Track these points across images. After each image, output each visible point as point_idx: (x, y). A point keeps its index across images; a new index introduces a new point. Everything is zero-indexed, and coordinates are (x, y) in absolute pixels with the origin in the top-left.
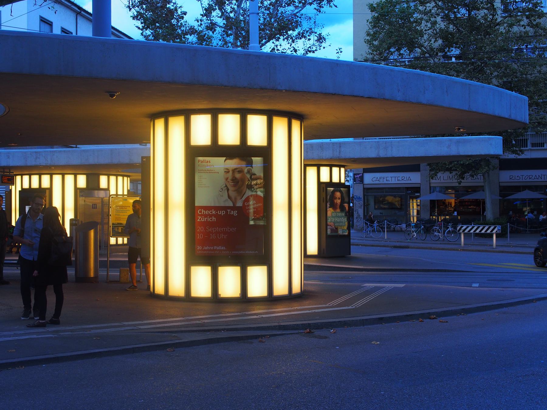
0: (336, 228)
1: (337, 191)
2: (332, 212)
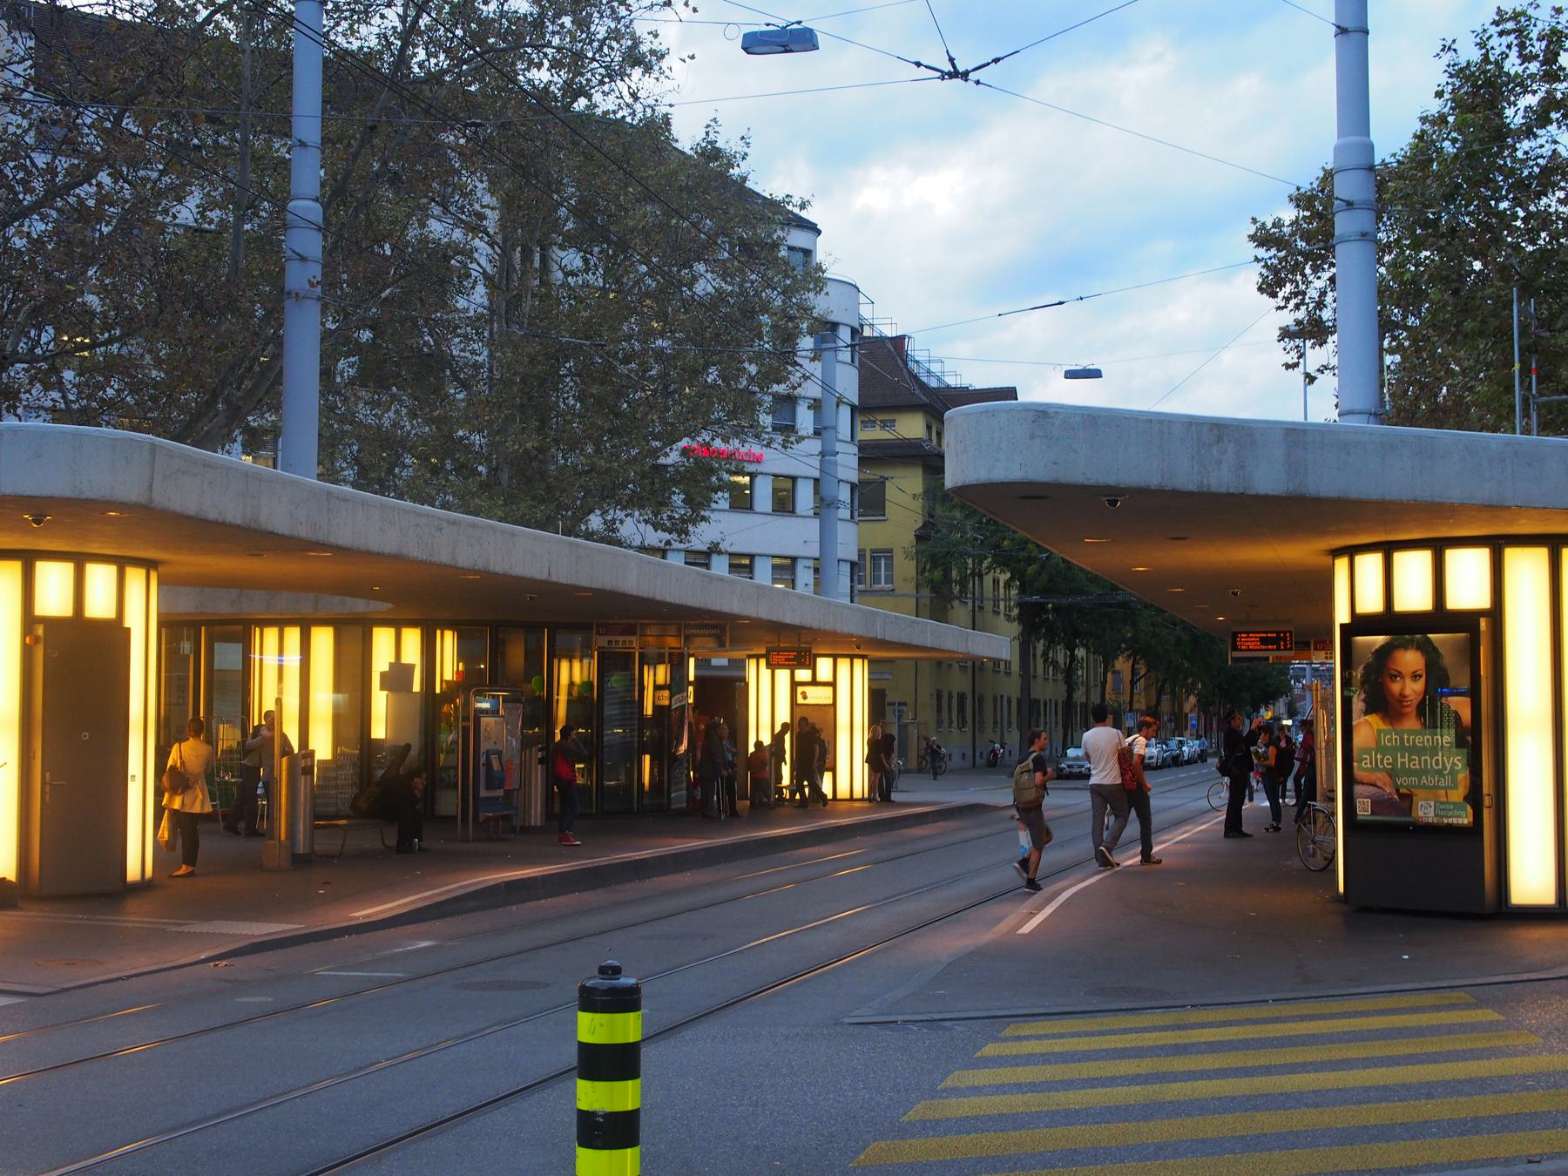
0: (1401, 796)
1: (1405, 646)
2: (1379, 731)
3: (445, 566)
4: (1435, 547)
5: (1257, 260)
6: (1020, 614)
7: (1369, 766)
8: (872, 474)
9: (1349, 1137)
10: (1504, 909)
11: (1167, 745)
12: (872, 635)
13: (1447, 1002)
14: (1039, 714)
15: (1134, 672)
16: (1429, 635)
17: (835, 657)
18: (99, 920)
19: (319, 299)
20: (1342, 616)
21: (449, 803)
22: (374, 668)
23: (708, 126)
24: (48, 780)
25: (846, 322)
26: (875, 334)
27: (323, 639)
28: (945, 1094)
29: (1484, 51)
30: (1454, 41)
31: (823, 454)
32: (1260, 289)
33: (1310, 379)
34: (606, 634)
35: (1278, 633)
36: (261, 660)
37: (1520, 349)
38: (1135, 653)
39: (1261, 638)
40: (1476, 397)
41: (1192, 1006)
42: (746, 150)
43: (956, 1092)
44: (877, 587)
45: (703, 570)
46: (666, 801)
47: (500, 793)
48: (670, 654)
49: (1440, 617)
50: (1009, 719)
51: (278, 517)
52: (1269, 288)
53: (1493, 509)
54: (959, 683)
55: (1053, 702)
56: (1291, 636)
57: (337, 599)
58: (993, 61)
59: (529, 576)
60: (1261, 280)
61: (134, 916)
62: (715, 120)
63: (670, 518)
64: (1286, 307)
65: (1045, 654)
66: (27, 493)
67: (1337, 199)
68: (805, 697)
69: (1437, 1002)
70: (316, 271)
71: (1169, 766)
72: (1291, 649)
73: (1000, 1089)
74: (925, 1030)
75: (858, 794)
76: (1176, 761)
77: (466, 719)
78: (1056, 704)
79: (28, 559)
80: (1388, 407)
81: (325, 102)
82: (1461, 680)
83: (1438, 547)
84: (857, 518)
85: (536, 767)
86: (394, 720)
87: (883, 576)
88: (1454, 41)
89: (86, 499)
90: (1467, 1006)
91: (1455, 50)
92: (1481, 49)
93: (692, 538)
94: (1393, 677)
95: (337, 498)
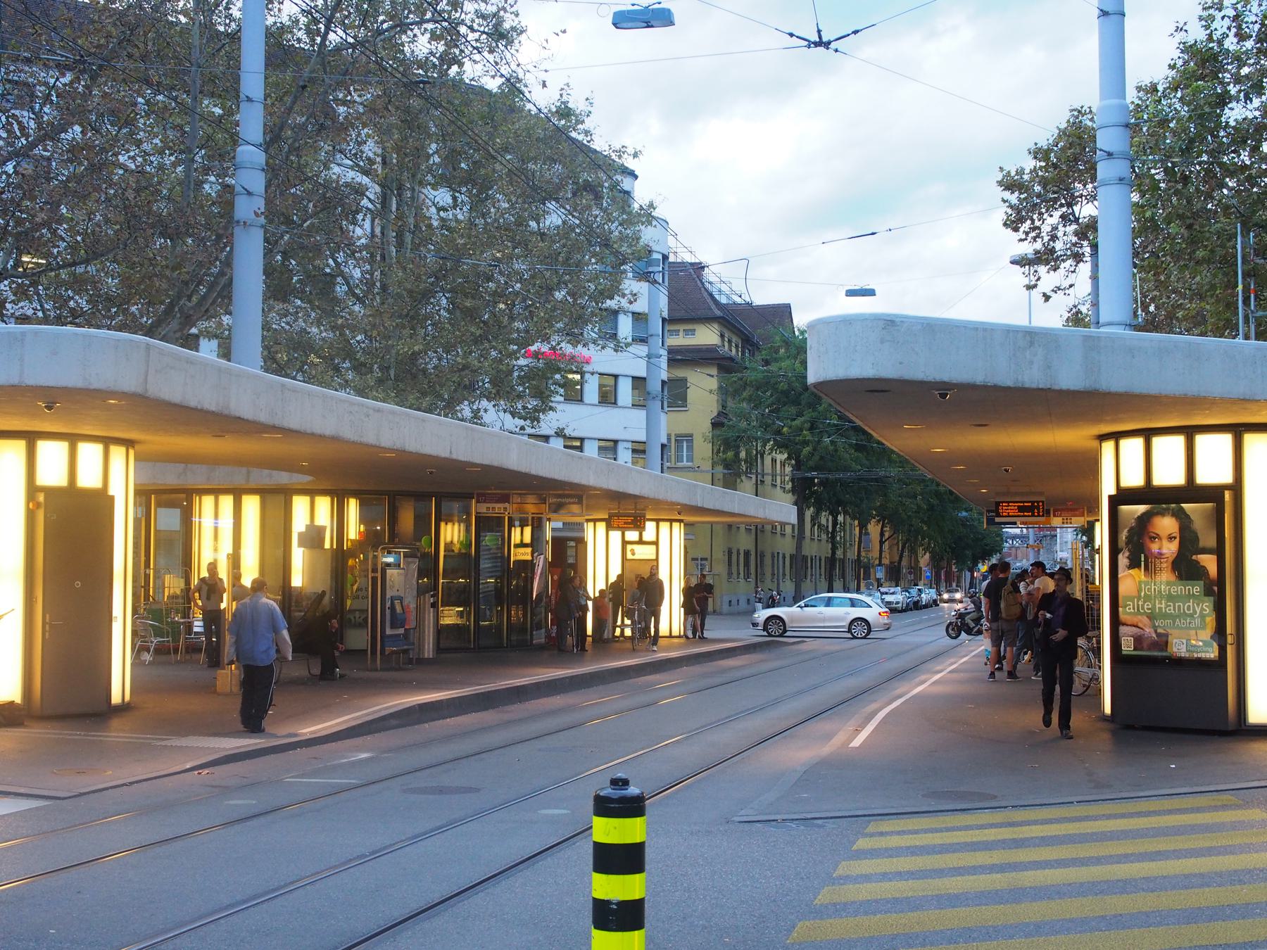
0: (1159, 635)
2: (1140, 582)
3: (372, 446)
4: (1187, 433)
5: (1005, 201)
6: (793, 487)
7: (1132, 610)
8: (680, 373)
9: (1192, 916)
10: (1243, 727)
11: (909, 593)
12: (693, 504)
13: (1220, 803)
14: (807, 568)
15: (882, 534)
16: (1182, 505)
17: (658, 521)
18: (94, 736)
19: (262, 226)
20: (1108, 488)
21: (358, 639)
22: (293, 530)
23: (562, 89)
24: (47, 620)
25: (658, 250)
26: (679, 260)
27: (251, 505)
28: (842, 881)
29: (1208, 32)
30: (1185, 23)
31: (649, 356)
32: (1005, 225)
33: (1047, 298)
34: (485, 502)
35: (1033, 502)
36: (200, 522)
37: (1243, 274)
38: (883, 519)
39: (1018, 506)
40: (1186, 312)
41: (1013, 807)
42: (590, 109)
43: (846, 879)
44: (680, 464)
45: (578, 453)
46: (529, 637)
47: (401, 631)
48: (533, 518)
49: (1191, 491)
50: (784, 571)
51: (244, 405)
52: (1013, 224)
53: (1244, 402)
54: (745, 542)
55: (818, 558)
56: (1043, 505)
57: (266, 472)
58: (853, 32)
59: (435, 455)
60: (1005, 218)
61: (117, 732)
62: (568, 85)
63: (524, 408)
64: (1026, 239)
65: (813, 519)
66: (46, 384)
67: (1101, 150)
68: (633, 554)
69: (1213, 804)
70: (260, 204)
71: (911, 610)
72: (1043, 515)
73: (885, 877)
74: (802, 827)
75: (675, 632)
76: (916, 606)
77: (375, 570)
78: (820, 560)
79: (31, 438)
80: (1140, 320)
81: (267, 65)
82: (1209, 540)
83: (1190, 432)
84: (666, 409)
85: (429, 611)
86: (311, 571)
87: (685, 455)
88: (1185, 23)
89: (94, 390)
90: (1238, 807)
91: (1186, 31)
92: (1207, 29)
93: (542, 423)
94: (1152, 539)
95: (289, 390)
